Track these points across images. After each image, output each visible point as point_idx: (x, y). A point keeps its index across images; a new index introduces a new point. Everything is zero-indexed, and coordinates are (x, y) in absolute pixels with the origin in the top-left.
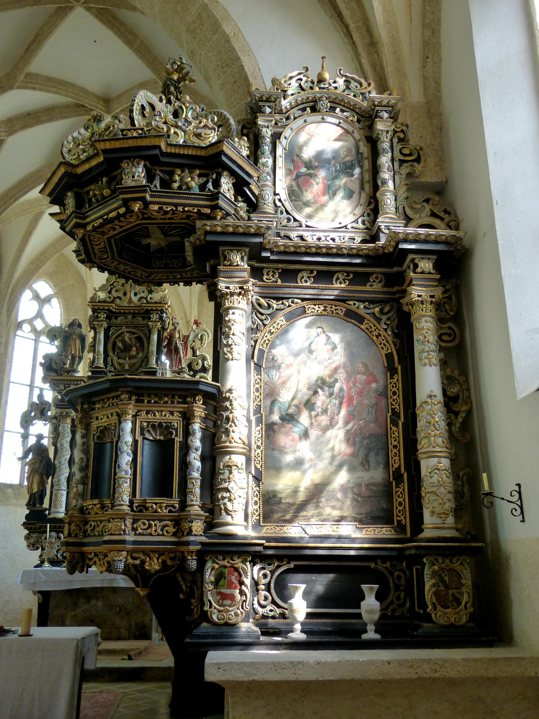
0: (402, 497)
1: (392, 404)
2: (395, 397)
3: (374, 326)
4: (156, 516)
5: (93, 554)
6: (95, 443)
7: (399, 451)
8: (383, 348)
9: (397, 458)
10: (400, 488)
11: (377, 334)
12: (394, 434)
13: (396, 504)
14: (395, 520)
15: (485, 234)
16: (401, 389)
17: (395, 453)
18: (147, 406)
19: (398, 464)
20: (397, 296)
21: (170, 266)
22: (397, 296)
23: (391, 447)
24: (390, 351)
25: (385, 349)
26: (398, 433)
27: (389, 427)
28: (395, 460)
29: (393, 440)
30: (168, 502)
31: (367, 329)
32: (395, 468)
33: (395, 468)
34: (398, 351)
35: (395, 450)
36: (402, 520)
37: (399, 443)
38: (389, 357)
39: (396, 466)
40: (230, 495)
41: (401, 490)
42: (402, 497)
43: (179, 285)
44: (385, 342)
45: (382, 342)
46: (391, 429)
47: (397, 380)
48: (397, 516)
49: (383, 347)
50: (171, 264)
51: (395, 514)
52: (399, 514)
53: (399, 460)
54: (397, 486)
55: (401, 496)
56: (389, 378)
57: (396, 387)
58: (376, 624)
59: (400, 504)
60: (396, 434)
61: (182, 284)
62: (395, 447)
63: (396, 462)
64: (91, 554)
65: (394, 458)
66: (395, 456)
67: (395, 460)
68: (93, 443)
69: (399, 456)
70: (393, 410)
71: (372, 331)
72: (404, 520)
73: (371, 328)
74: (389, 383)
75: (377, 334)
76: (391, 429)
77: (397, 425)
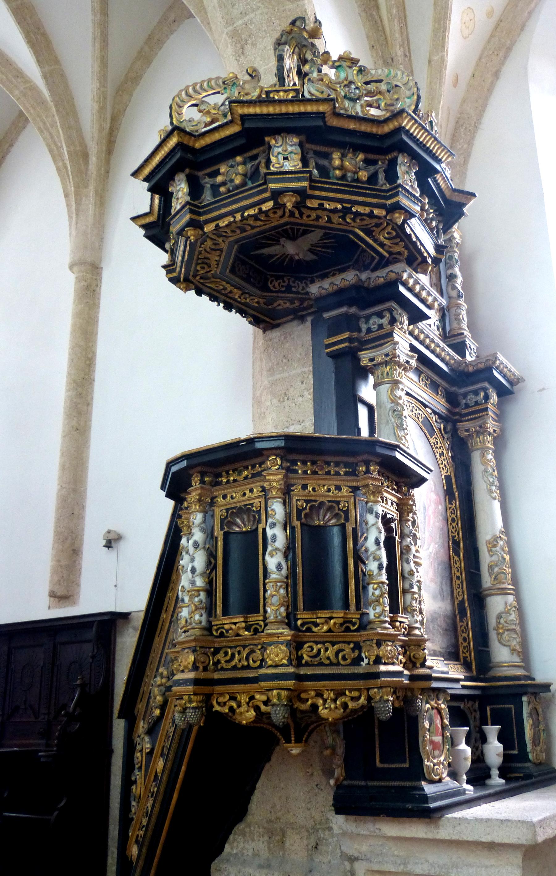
0: (466, 633)
1: (452, 532)
2: (454, 525)
3: (441, 443)
4: (239, 640)
5: (227, 697)
6: (302, 524)
7: (462, 582)
8: (443, 469)
9: (460, 590)
10: (463, 622)
11: (441, 452)
12: (456, 564)
13: (461, 640)
14: (462, 657)
15: (543, 389)
16: (459, 517)
17: (459, 584)
18: (302, 479)
19: (462, 597)
20: (456, 418)
21: (294, 289)
22: (456, 418)
23: (454, 578)
24: (449, 474)
25: (445, 471)
26: (460, 564)
27: (452, 556)
28: (459, 592)
29: (456, 570)
30: (256, 619)
31: (434, 443)
32: (459, 601)
33: (459, 601)
34: (455, 475)
35: (458, 582)
36: (467, 657)
37: (461, 574)
38: (448, 478)
39: (460, 598)
40: (422, 617)
41: (465, 624)
42: (466, 633)
43: (219, 305)
44: (445, 462)
45: (444, 462)
46: (454, 558)
47: (456, 506)
48: (463, 652)
49: (444, 468)
50: (295, 287)
51: (461, 650)
52: (465, 651)
53: (463, 592)
54: (461, 621)
55: (465, 631)
56: (448, 504)
57: (454, 514)
58: (500, 769)
59: (465, 639)
60: (458, 564)
61: (222, 305)
62: (458, 578)
63: (460, 594)
64: (224, 697)
65: (458, 590)
66: (459, 588)
67: (459, 592)
68: (298, 523)
69: (462, 588)
70: (453, 537)
71: (437, 447)
72: (469, 657)
73: (437, 444)
74: (448, 509)
75: (441, 452)
76: (454, 558)
77: (459, 556)
